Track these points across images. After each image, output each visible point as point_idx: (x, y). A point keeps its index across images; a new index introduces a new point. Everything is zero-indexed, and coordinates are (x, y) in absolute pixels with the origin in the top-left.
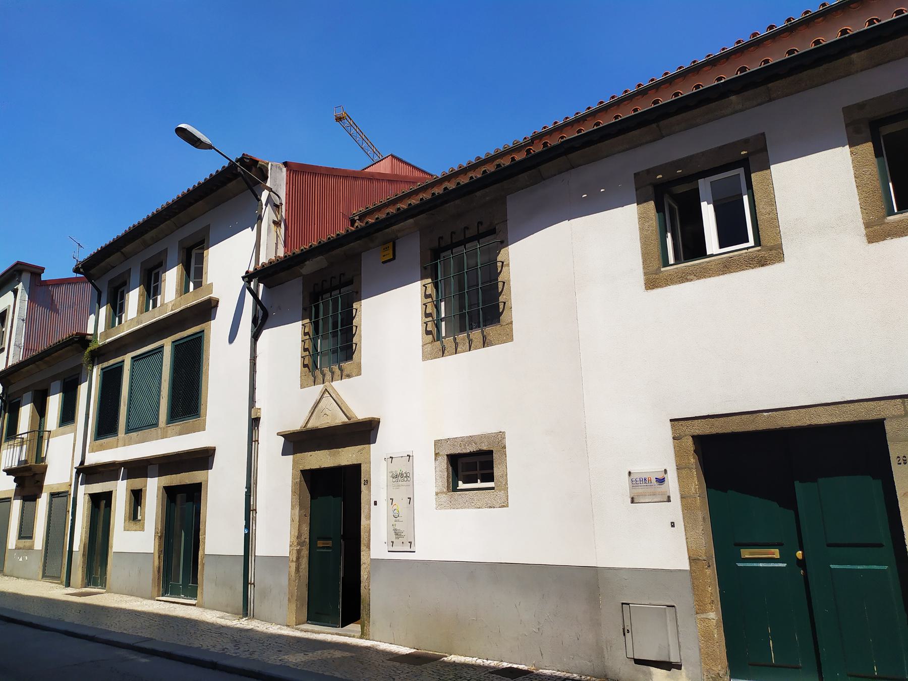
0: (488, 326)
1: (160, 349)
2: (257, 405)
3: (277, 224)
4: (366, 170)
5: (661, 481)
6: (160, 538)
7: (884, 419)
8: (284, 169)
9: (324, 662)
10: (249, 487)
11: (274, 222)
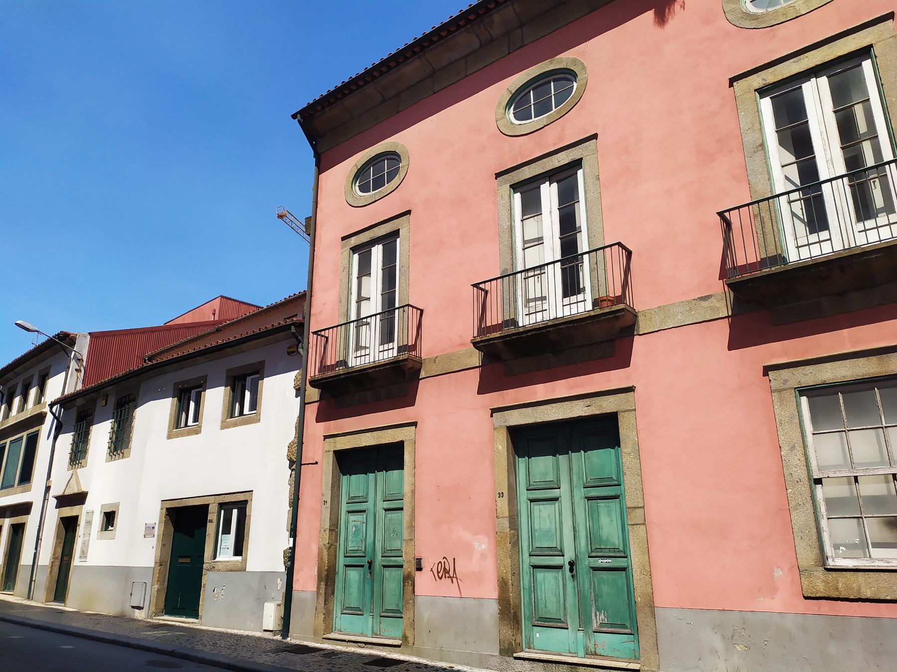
0: (749, 278)
1: (21, 438)
2: (51, 479)
3: (78, 371)
4: (168, 324)
5: (153, 528)
6: (5, 555)
7: (209, 504)
8: (89, 337)
9: (178, 637)
10: (40, 526)
11: (77, 370)
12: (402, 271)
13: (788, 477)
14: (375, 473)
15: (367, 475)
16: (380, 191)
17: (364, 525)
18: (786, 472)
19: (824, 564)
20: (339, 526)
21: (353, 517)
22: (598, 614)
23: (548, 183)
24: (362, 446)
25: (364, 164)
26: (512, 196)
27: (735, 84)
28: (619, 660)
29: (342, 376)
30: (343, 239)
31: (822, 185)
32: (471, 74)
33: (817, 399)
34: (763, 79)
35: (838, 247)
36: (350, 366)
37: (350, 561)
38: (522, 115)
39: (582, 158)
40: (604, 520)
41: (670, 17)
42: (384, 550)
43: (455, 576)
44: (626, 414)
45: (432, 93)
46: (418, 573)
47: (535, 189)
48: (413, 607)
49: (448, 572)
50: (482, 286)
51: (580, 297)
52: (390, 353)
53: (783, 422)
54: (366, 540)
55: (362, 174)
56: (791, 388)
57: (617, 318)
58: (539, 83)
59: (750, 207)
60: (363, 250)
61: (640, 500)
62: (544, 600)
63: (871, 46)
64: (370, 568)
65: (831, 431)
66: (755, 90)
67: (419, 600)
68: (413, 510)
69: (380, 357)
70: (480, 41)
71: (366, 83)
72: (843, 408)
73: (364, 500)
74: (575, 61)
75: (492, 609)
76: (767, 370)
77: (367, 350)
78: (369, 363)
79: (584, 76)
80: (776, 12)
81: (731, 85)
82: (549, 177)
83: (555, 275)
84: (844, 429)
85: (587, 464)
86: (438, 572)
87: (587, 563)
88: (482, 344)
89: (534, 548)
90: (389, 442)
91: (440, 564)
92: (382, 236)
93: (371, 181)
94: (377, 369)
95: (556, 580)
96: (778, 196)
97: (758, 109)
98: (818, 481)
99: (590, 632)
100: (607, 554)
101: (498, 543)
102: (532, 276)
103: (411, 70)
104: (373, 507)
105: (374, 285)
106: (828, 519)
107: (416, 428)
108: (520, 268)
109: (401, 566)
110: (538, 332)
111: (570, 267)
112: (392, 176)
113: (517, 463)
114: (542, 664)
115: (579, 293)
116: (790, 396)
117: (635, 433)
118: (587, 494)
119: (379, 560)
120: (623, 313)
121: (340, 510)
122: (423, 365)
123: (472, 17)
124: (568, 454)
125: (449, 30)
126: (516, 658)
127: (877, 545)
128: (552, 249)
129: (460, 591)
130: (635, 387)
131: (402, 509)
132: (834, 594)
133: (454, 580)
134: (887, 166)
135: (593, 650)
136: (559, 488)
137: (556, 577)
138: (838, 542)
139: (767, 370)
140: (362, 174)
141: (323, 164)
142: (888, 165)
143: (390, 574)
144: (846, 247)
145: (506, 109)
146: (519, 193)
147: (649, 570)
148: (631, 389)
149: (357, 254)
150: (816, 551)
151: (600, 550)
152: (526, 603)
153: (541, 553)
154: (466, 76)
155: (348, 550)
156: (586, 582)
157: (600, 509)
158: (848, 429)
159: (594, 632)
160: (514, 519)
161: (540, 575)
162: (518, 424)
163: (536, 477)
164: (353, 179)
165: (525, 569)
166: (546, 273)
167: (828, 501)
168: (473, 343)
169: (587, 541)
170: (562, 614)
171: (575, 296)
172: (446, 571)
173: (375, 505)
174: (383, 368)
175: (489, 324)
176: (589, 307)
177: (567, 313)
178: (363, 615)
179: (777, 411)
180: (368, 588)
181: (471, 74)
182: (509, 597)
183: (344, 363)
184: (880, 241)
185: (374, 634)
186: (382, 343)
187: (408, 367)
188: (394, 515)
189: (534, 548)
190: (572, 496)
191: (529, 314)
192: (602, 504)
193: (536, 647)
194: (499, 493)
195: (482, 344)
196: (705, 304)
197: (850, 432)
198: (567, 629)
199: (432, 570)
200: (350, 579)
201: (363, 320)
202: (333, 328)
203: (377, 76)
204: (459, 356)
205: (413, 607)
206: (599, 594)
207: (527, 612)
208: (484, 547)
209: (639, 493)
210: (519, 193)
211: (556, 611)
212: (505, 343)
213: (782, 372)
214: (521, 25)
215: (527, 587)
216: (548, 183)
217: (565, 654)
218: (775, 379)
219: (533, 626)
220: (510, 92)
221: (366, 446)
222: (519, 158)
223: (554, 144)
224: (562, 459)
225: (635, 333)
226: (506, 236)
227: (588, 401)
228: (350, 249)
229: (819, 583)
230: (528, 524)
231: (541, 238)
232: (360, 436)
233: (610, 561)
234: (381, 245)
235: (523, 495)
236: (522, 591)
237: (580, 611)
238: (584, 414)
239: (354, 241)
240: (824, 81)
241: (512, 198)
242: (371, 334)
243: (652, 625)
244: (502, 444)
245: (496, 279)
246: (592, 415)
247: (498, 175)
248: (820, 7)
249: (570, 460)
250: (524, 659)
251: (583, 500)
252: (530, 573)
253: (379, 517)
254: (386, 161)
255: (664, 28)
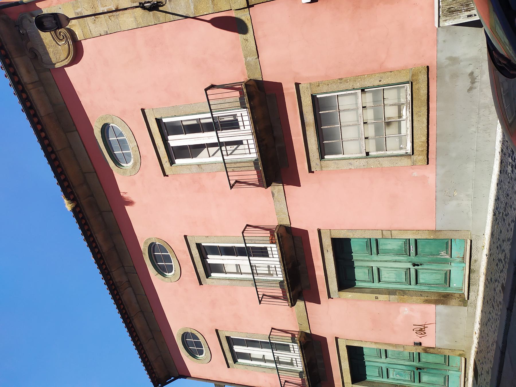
12: (249, 337)
13: (365, 167)
14: (365, 361)
15: (366, 366)
16: (203, 344)
17: (395, 370)
18: (362, 167)
19: (410, 155)
20: (396, 384)
21: (391, 376)
22: (441, 255)
23: (207, 260)
24: (349, 369)
25: (187, 352)
26: (213, 278)
27: (167, 174)
28: (466, 247)
29: (308, 377)
30: (229, 367)
31: (220, 141)
32: (145, 293)
33: (326, 151)
34: (166, 162)
35: (251, 137)
36: (302, 370)
37: (417, 379)
38: (170, 269)
39: (196, 243)
40: (389, 247)
41: (130, 199)
42: (409, 360)
43: (424, 326)
44: (332, 234)
45: (95, 173)
46: (423, 345)
47: (210, 267)
48: (442, 349)
49: (422, 329)
50: (260, 299)
51: (269, 249)
52: (296, 347)
53: (337, 167)
54: (404, 370)
55: (193, 353)
56: (320, 163)
57: (281, 237)
58: (154, 260)
59: (219, 137)
60: (236, 356)
61: (378, 231)
62: (435, 280)
63: (156, 119)
64: (420, 369)
65: (340, 133)
66: (171, 166)
67: (438, 345)
68: (386, 344)
69: (297, 353)
70: (128, 287)
71: (143, 348)
72: (329, 127)
73: (381, 368)
74: (146, 243)
75: (441, 308)
76: (310, 171)
77: (294, 359)
78: (301, 362)
79: (154, 239)
80: (134, 155)
81: (167, 176)
82: (204, 258)
83: (256, 260)
84: (341, 142)
85: (359, 252)
86: (422, 334)
87: (413, 257)
88: (293, 302)
89: (406, 282)
90: (347, 354)
91: (417, 333)
92: (229, 346)
93: (194, 340)
94: (305, 358)
95: (423, 273)
96: (224, 159)
97: (180, 166)
98: (367, 154)
99: (451, 259)
100: (408, 248)
101: (404, 302)
102: (256, 271)
103: (138, 324)
104: (385, 364)
105: (256, 352)
106: (386, 151)
107: (339, 338)
108: (251, 276)
109: (419, 353)
110: (287, 274)
111: (253, 253)
112: (195, 337)
113: (359, 287)
114: (470, 286)
115: (237, 120)
116: (323, 163)
117: (342, 231)
118: (375, 254)
119: (416, 364)
120: (279, 234)
121: (386, 383)
122: (303, 331)
123: (116, 292)
124: (353, 261)
125: (114, 289)
126: (468, 299)
127: (400, 132)
128: (243, 261)
129: (432, 324)
130: (318, 229)
131: (386, 350)
132: (426, 152)
133: (426, 326)
134: (214, 116)
135: (461, 259)
136: (372, 267)
137: (422, 273)
138: (399, 147)
139: (310, 171)
140: (193, 353)
141: (186, 375)
142: (213, 115)
143: (423, 358)
144: (251, 134)
145: (165, 277)
146: (211, 274)
147: (416, 231)
148: (319, 231)
149: (238, 360)
150: (403, 158)
151: (406, 251)
152: (437, 289)
153: (409, 279)
154: (146, 295)
155: (410, 380)
156: (424, 259)
157: (383, 248)
158: (341, 140)
159: (451, 257)
160: (391, 292)
161: (421, 280)
162: (337, 286)
163: (366, 278)
164: (196, 359)
165: (419, 288)
166: (255, 264)
167: (377, 150)
168: (292, 307)
169: (401, 256)
170: (442, 272)
171: (268, 251)
172: (421, 330)
173: (383, 363)
174: (304, 355)
175: (282, 295)
176: (274, 245)
177: (277, 256)
178: (448, 376)
179: (332, 169)
180: (432, 371)
181: (145, 293)
182: (434, 299)
183: (301, 373)
184: (250, 125)
185: (459, 370)
186: (290, 351)
187: (304, 340)
188: (389, 353)
189: (406, 282)
190: (377, 261)
191: (277, 274)
192: (380, 247)
193: (461, 286)
194: (376, 299)
195: (293, 302)
196: (276, 195)
197: (341, 124)
198: (450, 270)
199: (421, 337)
200: (428, 381)
201: (276, 360)
202: (279, 377)
203: (140, 342)
204: (298, 312)
205: (442, 349)
206: (430, 253)
207: (442, 289)
208: (406, 309)
209: (374, 231)
210: (211, 274)
211: (441, 275)
212: (292, 290)
213: (312, 166)
214: (123, 266)
215: (428, 288)
216: (207, 260)
217: (464, 273)
218: (316, 169)
219: (450, 287)
220: (157, 274)
221: (349, 366)
222: (193, 272)
223: (187, 255)
224: (356, 264)
225: (289, 226)
226: (234, 282)
227: (325, 252)
228: (234, 363)
229: (420, 157)
230: (392, 284)
231: (236, 265)
232: (343, 369)
233: (411, 246)
234: (234, 346)
235: (376, 285)
236: (431, 291)
237: (440, 263)
238: (332, 254)
239: (231, 361)
240: (170, 137)
241: (214, 278)
242: (283, 356)
243: (446, 232)
244: (347, 295)
245: (256, 289)
246: (333, 250)
247: (201, 284)
248: (134, 137)
249: (357, 260)
250: (468, 295)
251: (378, 256)
252: (420, 286)
253: (391, 362)
254: (187, 340)
255: (135, 202)
